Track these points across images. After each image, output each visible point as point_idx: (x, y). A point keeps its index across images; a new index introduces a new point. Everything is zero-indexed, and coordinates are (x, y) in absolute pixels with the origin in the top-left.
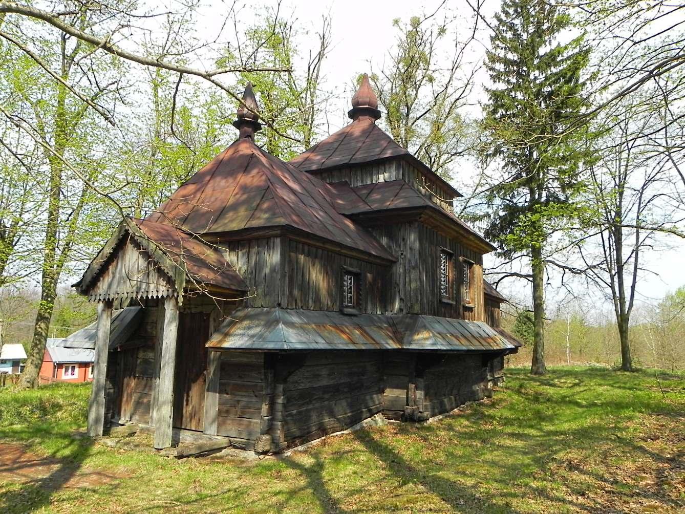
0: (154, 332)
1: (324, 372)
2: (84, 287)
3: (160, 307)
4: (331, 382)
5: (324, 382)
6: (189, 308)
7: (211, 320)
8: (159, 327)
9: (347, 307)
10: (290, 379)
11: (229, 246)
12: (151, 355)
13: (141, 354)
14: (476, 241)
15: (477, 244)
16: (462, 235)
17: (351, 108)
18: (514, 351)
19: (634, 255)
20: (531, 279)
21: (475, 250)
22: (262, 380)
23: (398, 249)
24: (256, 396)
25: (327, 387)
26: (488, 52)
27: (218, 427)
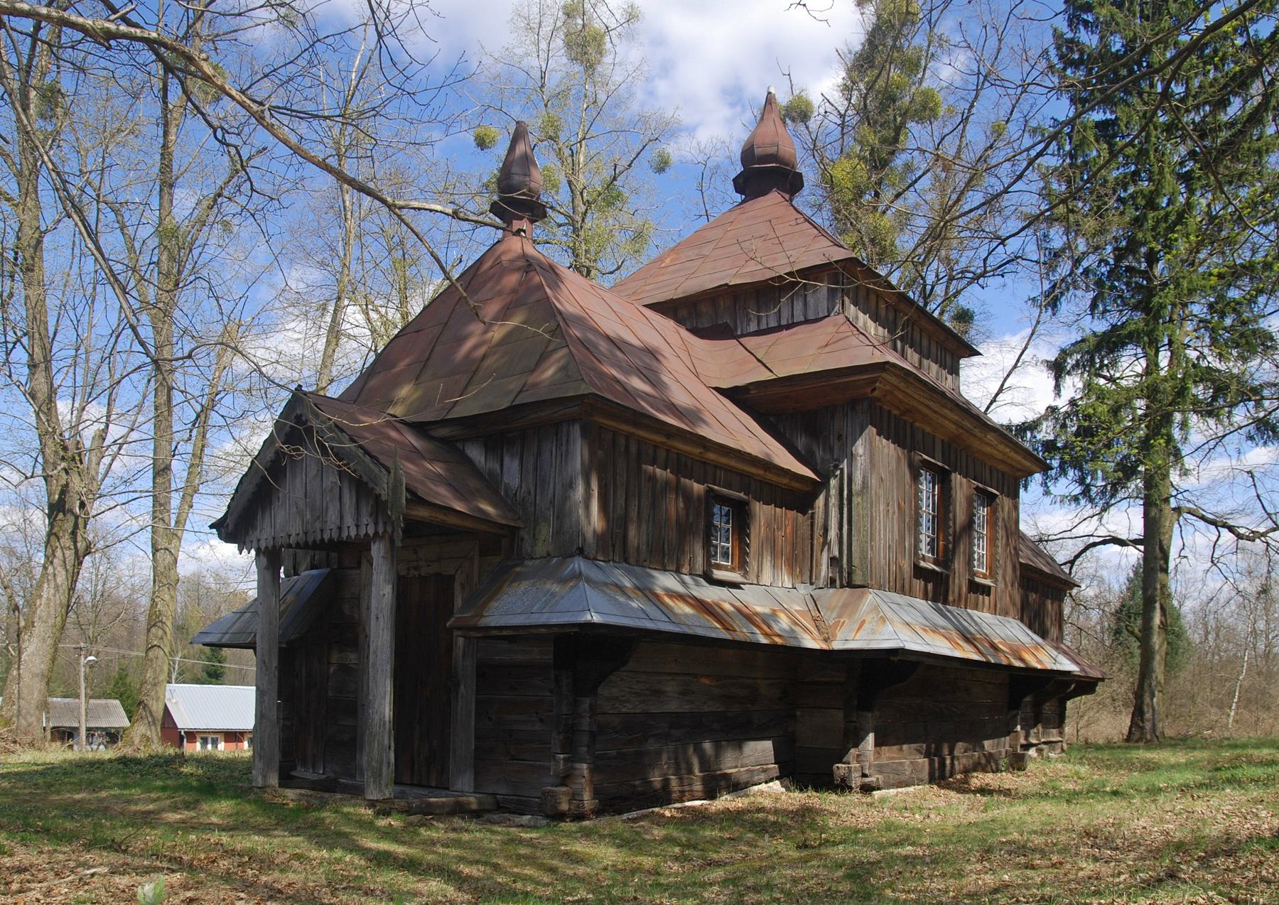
0: (356, 616)
1: (671, 688)
2: (231, 527)
3: (364, 566)
4: (687, 708)
5: (673, 706)
6: (416, 568)
7: (457, 587)
8: (364, 606)
9: (719, 567)
10: (603, 691)
11: (486, 446)
12: (352, 657)
13: (335, 657)
14: (1001, 447)
15: (1005, 454)
16: (967, 431)
17: (740, 169)
18: (1086, 685)
19: (961, 127)
20: (1142, 548)
21: (1000, 467)
22: (551, 691)
23: (828, 456)
24: (541, 721)
25: (678, 715)
26: (1057, 35)
27: (475, 780)
